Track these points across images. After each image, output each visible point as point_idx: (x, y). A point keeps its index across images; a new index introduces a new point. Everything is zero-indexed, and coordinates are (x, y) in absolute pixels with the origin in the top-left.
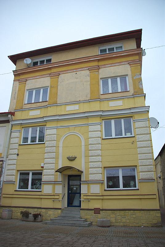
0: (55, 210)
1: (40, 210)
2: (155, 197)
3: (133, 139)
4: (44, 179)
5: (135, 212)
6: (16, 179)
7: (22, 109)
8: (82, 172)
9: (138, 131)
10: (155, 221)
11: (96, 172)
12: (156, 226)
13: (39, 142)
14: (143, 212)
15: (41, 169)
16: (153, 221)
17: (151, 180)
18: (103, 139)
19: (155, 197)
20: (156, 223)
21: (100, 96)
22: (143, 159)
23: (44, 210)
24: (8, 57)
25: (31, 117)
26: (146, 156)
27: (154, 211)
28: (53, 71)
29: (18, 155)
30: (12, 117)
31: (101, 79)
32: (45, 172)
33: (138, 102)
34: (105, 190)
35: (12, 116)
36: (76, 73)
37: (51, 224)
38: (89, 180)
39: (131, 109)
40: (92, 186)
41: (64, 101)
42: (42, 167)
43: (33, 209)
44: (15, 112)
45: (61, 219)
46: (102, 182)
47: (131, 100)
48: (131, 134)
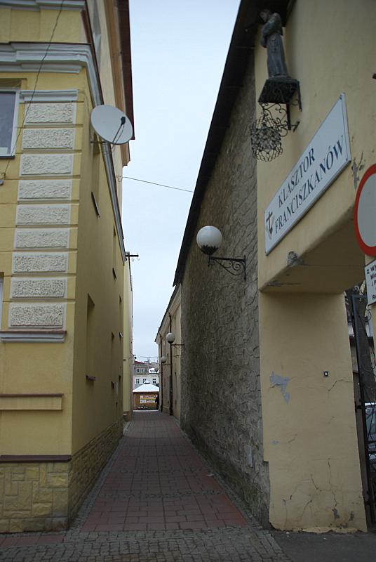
2: (56, 404)
9: (32, 138)
10: (41, 505)
12: (41, 526)
16: (35, 506)
17: (50, 333)
19: (56, 404)
20: (48, 516)
26: (47, 238)
27: (43, 465)
33: (252, 48)
37: (88, 493)
39: (16, 47)
48: (9, 152)
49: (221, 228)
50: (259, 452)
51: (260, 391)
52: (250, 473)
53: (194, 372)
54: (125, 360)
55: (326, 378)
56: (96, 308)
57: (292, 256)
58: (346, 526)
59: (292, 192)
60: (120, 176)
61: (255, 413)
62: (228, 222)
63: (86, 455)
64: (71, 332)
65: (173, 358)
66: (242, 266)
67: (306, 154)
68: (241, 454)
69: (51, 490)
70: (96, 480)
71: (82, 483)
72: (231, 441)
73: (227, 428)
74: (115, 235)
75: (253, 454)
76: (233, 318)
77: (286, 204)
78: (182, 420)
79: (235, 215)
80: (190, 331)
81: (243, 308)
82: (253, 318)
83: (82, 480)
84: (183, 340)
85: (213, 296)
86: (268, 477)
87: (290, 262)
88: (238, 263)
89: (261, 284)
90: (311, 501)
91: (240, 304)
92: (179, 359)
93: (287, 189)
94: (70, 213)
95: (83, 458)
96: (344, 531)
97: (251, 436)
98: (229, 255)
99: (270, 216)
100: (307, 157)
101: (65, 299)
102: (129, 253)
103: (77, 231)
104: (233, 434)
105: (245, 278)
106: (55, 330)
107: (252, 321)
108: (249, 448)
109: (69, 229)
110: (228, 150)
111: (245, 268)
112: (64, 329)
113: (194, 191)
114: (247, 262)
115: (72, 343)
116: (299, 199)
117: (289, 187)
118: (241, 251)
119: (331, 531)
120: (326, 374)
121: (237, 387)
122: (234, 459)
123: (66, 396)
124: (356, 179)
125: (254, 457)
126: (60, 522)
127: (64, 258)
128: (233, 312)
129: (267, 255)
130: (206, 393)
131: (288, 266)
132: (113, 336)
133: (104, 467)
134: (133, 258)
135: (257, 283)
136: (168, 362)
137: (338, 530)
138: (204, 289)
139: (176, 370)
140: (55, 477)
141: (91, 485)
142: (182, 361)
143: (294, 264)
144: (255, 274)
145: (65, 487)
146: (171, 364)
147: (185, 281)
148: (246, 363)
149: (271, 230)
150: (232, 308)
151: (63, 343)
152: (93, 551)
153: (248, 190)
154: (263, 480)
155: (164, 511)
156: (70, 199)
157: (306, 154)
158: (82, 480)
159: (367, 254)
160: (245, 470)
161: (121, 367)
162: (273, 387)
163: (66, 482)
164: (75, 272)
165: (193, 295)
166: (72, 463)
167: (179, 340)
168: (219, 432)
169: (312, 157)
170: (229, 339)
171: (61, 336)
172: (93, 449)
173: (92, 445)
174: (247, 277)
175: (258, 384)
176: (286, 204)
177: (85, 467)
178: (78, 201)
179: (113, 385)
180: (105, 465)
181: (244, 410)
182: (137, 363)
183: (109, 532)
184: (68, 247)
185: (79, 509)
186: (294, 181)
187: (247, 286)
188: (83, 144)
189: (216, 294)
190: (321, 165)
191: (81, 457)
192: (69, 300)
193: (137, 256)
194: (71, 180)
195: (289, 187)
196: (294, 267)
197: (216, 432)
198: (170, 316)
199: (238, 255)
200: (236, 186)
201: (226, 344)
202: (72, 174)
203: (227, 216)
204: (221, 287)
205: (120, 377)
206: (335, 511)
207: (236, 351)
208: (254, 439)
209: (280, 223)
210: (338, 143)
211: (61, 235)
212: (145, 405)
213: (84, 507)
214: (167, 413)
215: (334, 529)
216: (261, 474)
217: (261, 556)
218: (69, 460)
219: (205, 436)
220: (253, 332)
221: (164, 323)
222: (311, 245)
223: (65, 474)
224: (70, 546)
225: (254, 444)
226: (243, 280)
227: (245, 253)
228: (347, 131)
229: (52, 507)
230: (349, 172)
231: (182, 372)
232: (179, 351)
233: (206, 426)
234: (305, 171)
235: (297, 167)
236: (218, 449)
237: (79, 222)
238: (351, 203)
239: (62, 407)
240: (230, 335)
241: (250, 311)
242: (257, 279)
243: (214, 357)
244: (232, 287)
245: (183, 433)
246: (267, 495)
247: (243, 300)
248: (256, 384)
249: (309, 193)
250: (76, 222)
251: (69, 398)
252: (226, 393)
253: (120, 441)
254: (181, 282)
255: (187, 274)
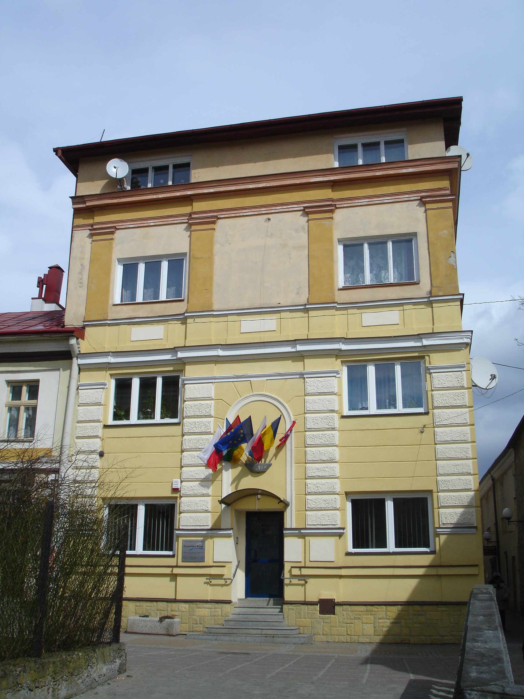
0: (217, 605)
1: (174, 605)
3: (424, 420)
4: (182, 523)
5: (425, 608)
6: (344, 520)
7: (102, 323)
8: (287, 505)
11: (323, 506)
13: (162, 418)
14: (445, 609)
15: (169, 494)
18: (343, 417)
21: (337, 293)
22: (448, 475)
23: (186, 606)
24: (56, 150)
25: (136, 344)
28: (198, 206)
29: (101, 454)
30: (78, 344)
31: (340, 241)
32: (184, 503)
34: (348, 554)
35: (80, 339)
36: (269, 219)
38: (307, 527)
39: (422, 336)
40: (314, 541)
41: (235, 303)
42: (176, 490)
43: (155, 603)
44: (87, 329)
45: (234, 627)
46: (341, 531)
47: (177, 327)
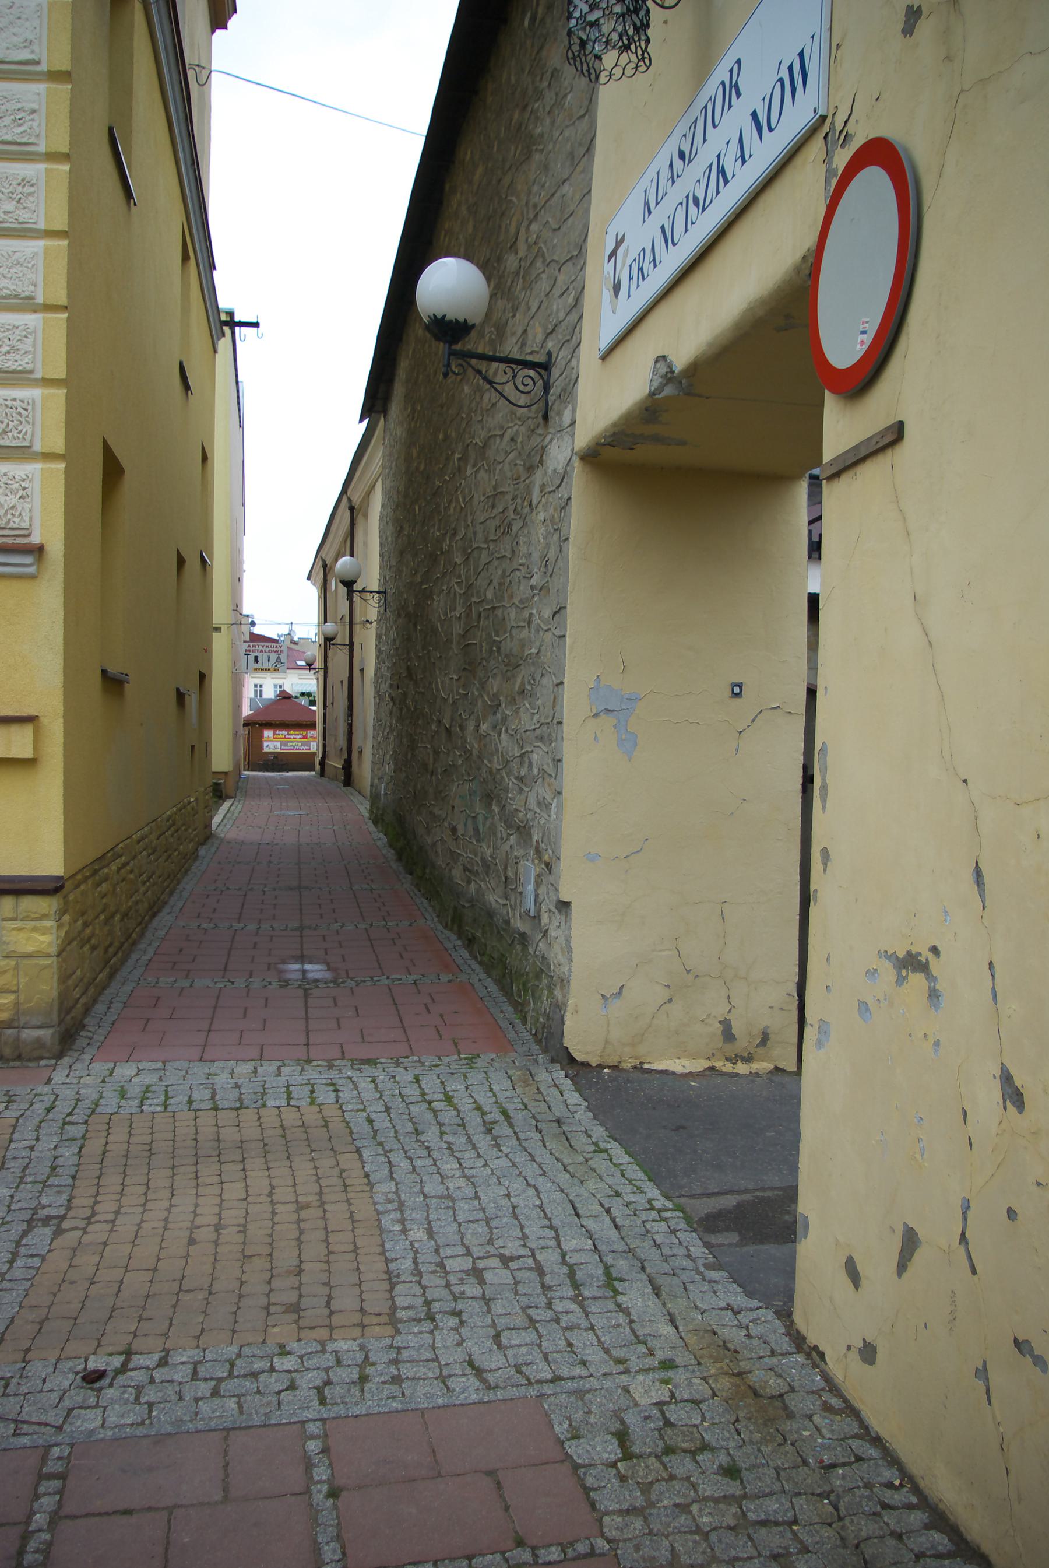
49: (486, 267)
50: (552, 879)
51: (560, 723)
52: (528, 932)
53: (408, 669)
54: (218, 629)
55: (738, 701)
56: (130, 483)
57: (663, 369)
58: (748, 1059)
59: (678, 181)
60: (205, 70)
61: (547, 780)
62: (513, 248)
63: (106, 879)
64: (56, 548)
65: (357, 628)
66: (540, 383)
67: (721, 74)
68: (510, 885)
69: (13, 963)
70: (134, 943)
71: (94, 948)
72: (488, 852)
73: (480, 818)
74: (185, 258)
75: (538, 884)
76: (510, 527)
77: (660, 216)
78: (375, 797)
79: (534, 227)
80: (401, 553)
81: (534, 503)
82: (558, 529)
83: (93, 941)
84: (384, 580)
85: (464, 459)
86: (568, 940)
87: (656, 384)
88: (532, 373)
89: (584, 435)
90: (670, 1001)
91: (528, 490)
92: (372, 632)
93: (665, 174)
94: (43, 197)
95: (99, 885)
96: (742, 1068)
97: (535, 838)
98: (511, 348)
99: (618, 244)
100: (723, 83)
101: (36, 454)
102: (231, 314)
103: (64, 254)
104: (495, 834)
105: (546, 417)
106: (10, 541)
107: (556, 537)
108: (530, 869)
109: (41, 243)
110: (528, 15)
111: (547, 387)
112: (36, 539)
113: (425, 133)
114: (555, 372)
115: (60, 577)
116: (692, 209)
117: (671, 165)
118: (540, 337)
119: (712, 1069)
120: (737, 690)
121: (508, 712)
122: (493, 898)
123: (44, 721)
124: (829, 173)
125: (540, 891)
126: (38, 1040)
127: (28, 405)
128: (511, 508)
129: (604, 358)
130: (434, 727)
131: (652, 394)
132: (181, 561)
133: (154, 915)
134: (244, 329)
135: (573, 436)
136: (343, 638)
137: (728, 1067)
138: (441, 436)
139: (362, 660)
140: (20, 929)
141: (120, 954)
142: (379, 637)
143: (668, 391)
144: (570, 407)
145: (49, 956)
146: (351, 645)
147: (395, 408)
148: (534, 651)
149: (617, 288)
150: (509, 497)
151: (33, 577)
152: (123, 1103)
153: (571, 155)
154: (556, 948)
155: (307, 1018)
156: (42, 148)
157: (721, 74)
158: (93, 941)
159: (834, 391)
160: (518, 924)
161: (207, 650)
162: (596, 715)
163: (50, 944)
164: (64, 376)
165: (415, 452)
166: (65, 897)
167: (372, 578)
168: (460, 831)
169: (736, 86)
170: (495, 583)
171: (28, 560)
172: (125, 865)
173: (120, 856)
174: (551, 414)
175: (558, 708)
176: (660, 216)
177: (104, 911)
178: (66, 157)
179: (180, 697)
180: (159, 911)
181: (523, 772)
182: (256, 638)
183: (164, 1062)
184: (40, 300)
185: (87, 1011)
186: (686, 149)
187: (549, 437)
188: (75, 48)
189: (472, 454)
190: (754, 115)
191: (90, 882)
192: (47, 457)
193: (256, 325)
194: (41, 87)
195: (671, 165)
196: (666, 398)
197: (454, 830)
198: (352, 509)
199: (534, 350)
200: (541, 135)
201: (489, 595)
202: (44, 67)
203: (513, 230)
204: (483, 434)
205: (202, 677)
206: (726, 1025)
207: (513, 615)
208: (542, 845)
209: (641, 269)
210: (801, 55)
211: (19, 263)
212: (276, 755)
213: (100, 1008)
214: (335, 778)
215: (719, 1064)
216: (553, 933)
217: (534, 1117)
218: (56, 890)
219: (429, 840)
220: (552, 566)
221: (334, 527)
222: (710, 345)
223: (48, 923)
224: (68, 1092)
225: (540, 858)
226: (540, 420)
227: (550, 345)
228: (826, 26)
229: (17, 1004)
230: (816, 147)
231: (378, 669)
232: (371, 609)
233: (431, 812)
234: (715, 126)
235: (696, 111)
236: (457, 873)
237: (70, 224)
238: (810, 241)
239: (36, 748)
240: (500, 572)
241: (551, 510)
242: (573, 423)
243: (458, 629)
244: (512, 439)
245: (380, 838)
246: (564, 982)
247: (538, 478)
248: (554, 707)
249: (718, 192)
250: (61, 223)
251: (55, 728)
252: (484, 727)
253: (202, 852)
254: (385, 412)
255: (399, 390)
